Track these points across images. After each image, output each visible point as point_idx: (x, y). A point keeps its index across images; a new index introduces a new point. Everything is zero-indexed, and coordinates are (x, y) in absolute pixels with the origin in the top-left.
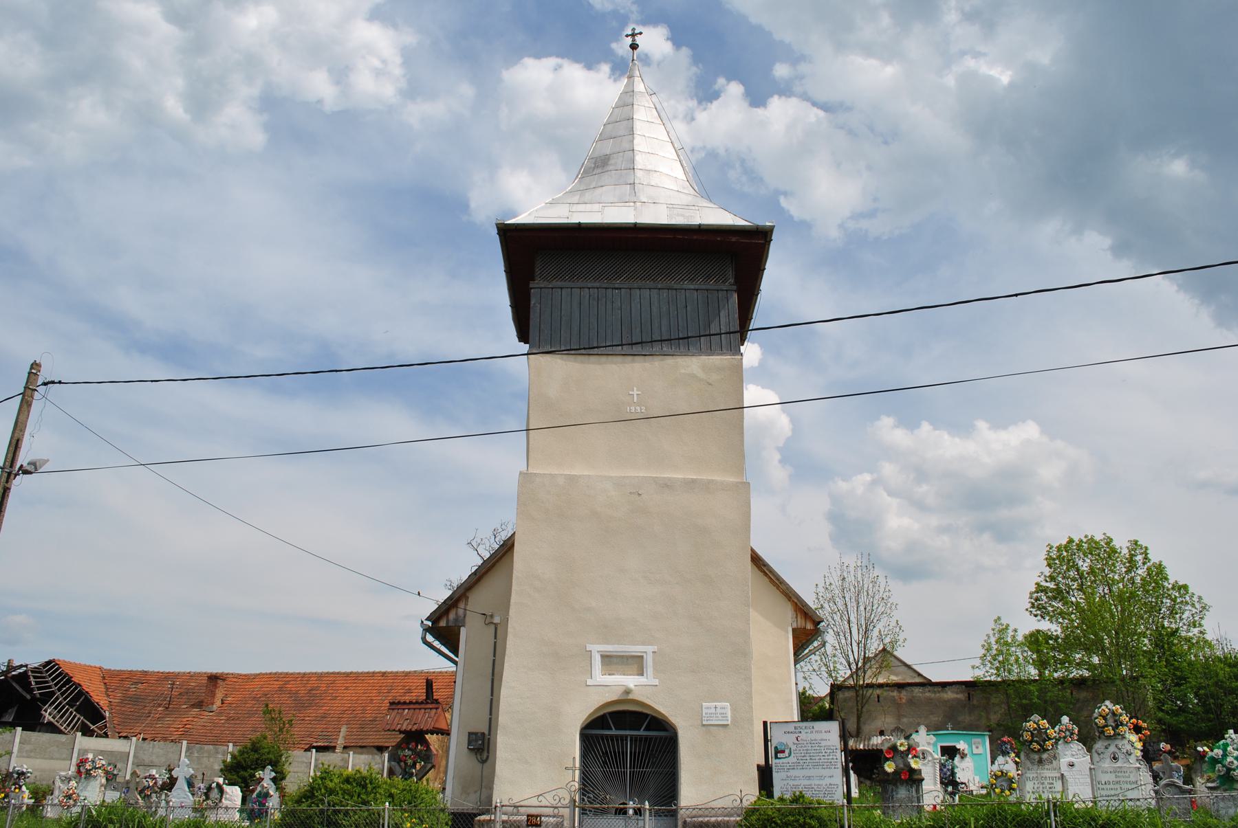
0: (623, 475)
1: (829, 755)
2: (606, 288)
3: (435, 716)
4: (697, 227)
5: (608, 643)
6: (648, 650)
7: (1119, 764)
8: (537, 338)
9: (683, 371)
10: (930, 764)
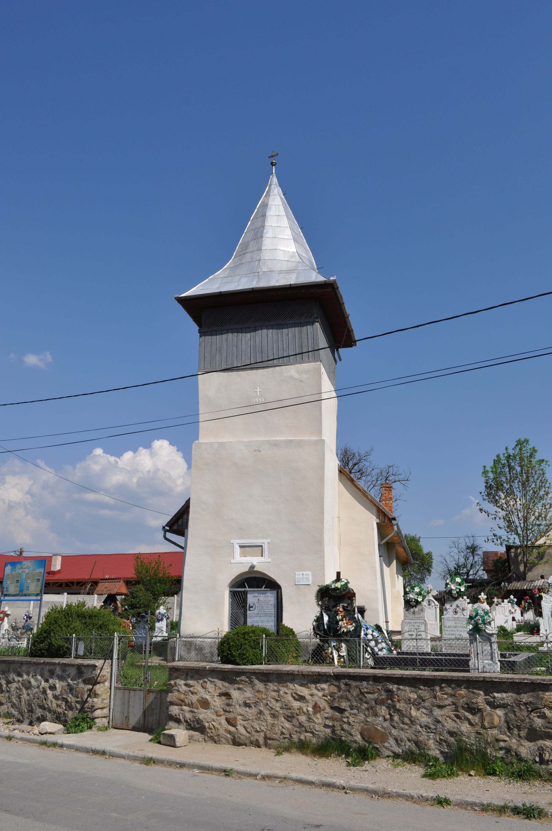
2: (242, 328)
5: (242, 539)
6: (265, 542)
7: (457, 616)
8: (203, 362)
9: (286, 375)
10: (434, 607)
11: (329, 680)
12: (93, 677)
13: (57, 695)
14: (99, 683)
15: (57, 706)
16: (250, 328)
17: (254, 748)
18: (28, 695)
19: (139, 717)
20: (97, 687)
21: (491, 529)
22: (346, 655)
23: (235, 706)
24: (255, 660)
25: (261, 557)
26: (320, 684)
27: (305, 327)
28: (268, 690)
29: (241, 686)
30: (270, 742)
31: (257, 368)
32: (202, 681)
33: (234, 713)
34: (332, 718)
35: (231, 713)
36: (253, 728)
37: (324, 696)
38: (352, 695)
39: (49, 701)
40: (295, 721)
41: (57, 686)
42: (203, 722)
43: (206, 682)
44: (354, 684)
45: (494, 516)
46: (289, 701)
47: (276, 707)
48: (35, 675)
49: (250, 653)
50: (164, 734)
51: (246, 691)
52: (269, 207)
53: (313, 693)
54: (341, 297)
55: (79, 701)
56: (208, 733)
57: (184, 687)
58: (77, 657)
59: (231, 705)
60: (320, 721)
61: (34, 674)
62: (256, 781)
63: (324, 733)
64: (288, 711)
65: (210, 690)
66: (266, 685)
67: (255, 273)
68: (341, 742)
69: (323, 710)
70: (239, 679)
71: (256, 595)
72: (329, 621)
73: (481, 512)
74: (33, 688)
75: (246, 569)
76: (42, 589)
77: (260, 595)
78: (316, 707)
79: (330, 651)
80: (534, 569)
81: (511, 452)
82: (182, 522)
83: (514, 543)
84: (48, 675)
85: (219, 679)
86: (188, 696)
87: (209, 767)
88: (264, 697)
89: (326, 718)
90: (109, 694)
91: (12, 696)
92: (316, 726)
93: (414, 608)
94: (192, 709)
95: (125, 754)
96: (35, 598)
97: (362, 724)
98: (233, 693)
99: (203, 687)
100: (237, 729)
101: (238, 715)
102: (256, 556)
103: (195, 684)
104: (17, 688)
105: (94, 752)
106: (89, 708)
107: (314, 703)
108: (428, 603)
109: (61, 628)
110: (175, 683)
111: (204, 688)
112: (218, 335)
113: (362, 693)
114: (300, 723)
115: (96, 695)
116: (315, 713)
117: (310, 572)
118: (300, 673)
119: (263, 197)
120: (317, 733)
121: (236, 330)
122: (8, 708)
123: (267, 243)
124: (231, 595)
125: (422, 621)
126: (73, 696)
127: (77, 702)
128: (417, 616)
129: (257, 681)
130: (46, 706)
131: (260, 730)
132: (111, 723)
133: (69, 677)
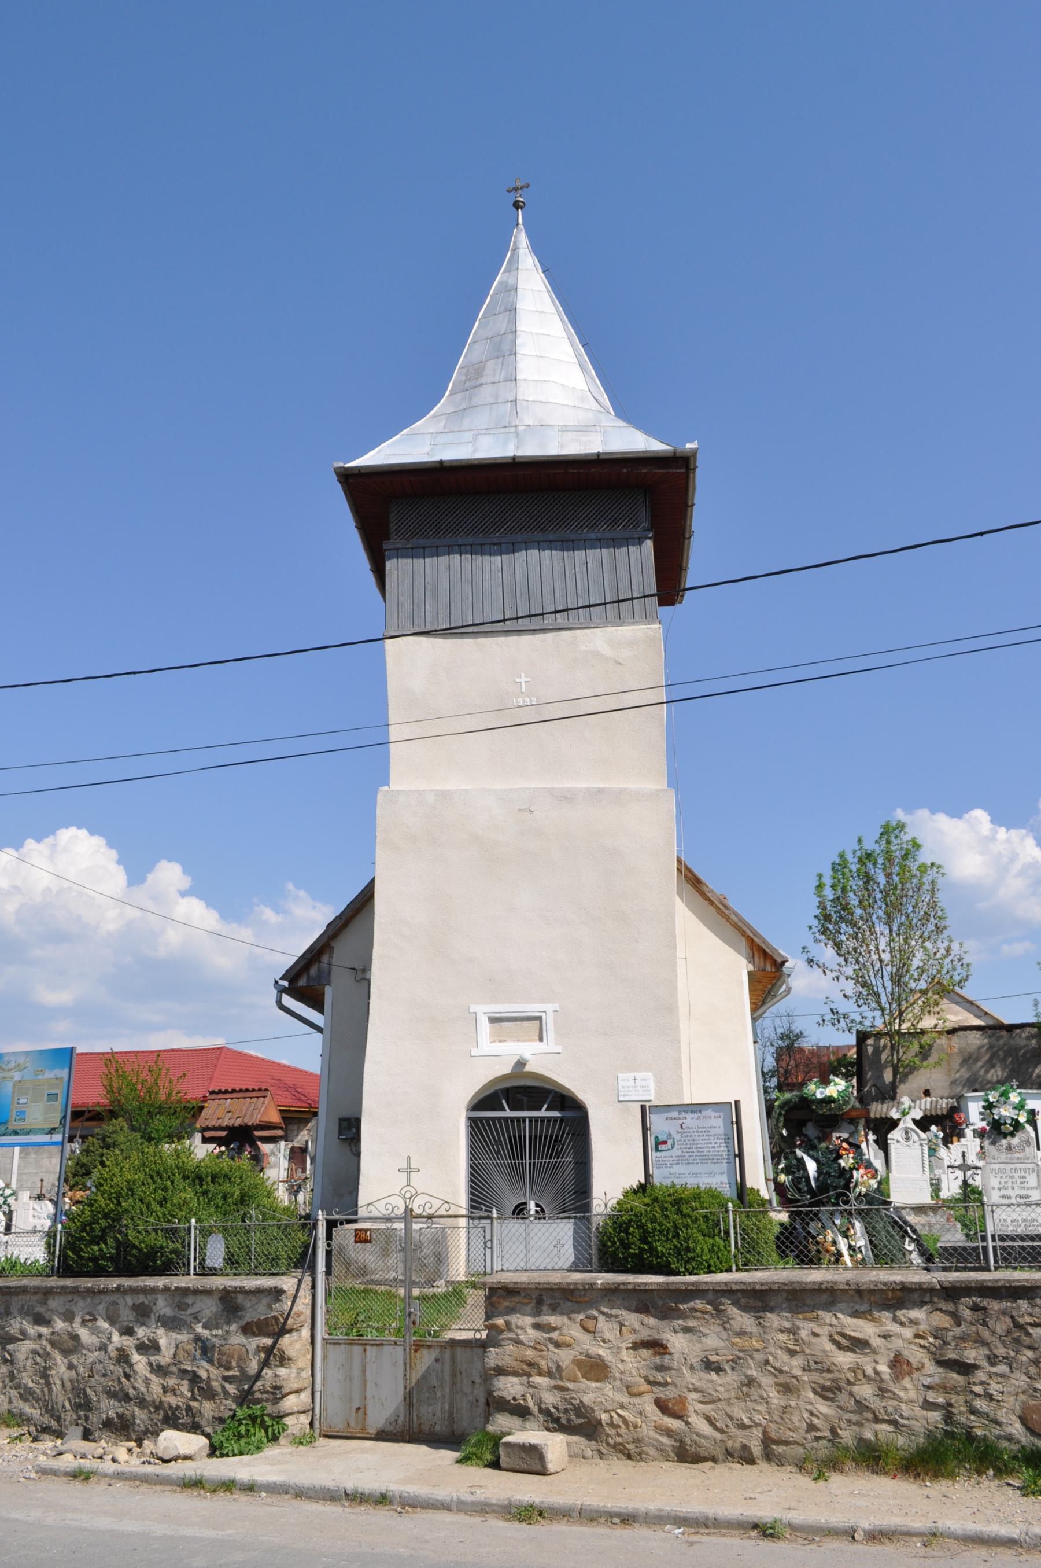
0: (511, 787)
1: (720, 1147)
2: (482, 545)
3: (262, 1107)
4: (595, 457)
6: (547, 1010)
9: (583, 648)
10: (917, 1145)
11: (927, 1299)
12: (275, 1318)
13: (162, 1364)
14: (290, 1331)
15: (165, 1392)
16: (500, 544)
17: (739, 1465)
18: (71, 1367)
19: (393, 1408)
20: (286, 1341)
21: (826, 1000)
22: (865, 1246)
23: (679, 1370)
24: (715, 1263)
25: (538, 1043)
26: (904, 1311)
27: (624, 550)
28: (767, 1330)
29: (691, 1323)
30: (780, 1449)
31: (520, 632)
32: (582, 1316)
33: (676, 1386)
34: (944, 1388)
35: (669, 1387)
36: (731, 1418)
37: (917, 1336)
38: (994, 1332)
39: (140, 1381)
40: (843, 1398)
41: (163, 1342)
42: (594, 1411)
43: (596, 1318)
44: (995, 1306)
45: (835, 974)
46: (824, 1351)
47: (792, 1368)
48: (90, 1320)
49: (702, 1245)
50: (508, 1445)
51: (705, 1335)
52: (519, 291)
53: (887, 1331)
54: (694, 489)
55: (233, 1377)
56: (608, 1435)
57: (530, 1331)
58: (205, 1271)
59: (669, 1369)
60: (912, 1394)
61: (88, 1317)
62: (855, 1546)
63: (925, 1422)
64: (825, 1375)
65: (608, 1335)
66: (758, 1318)
67: (507, 428)
68: (970, 1437)
69: (918, 1369)
70: (685, 1306)
71: (675, 1114)
72: (819, 1171)
73: (811, 966)
74: (84, 1352)
75: (507, 1069)
76: (64, 1117)
77: (684, 1115)
78: (898, 1362)
79: (830, 1238)
80: (910, 1077)
81: (869, 845)
82: (319, 969)
83: (873, 1026)
84: (131, 1318)
85: (630, 1310)
86: (545, 1353)
87: (707, 1518)
88: (757, 1345)
89: (929, 1387)
90: (309, 1357)
91: (19, 1372)
92: (903, 1406)
93: (1009, 1138)
94: (560, 1383)
95: (448, 1498)
96: (46, 1138)
97: (1022, 1397)
98: (672, 1339)
99: (586, 1329)
100: (687, 1423)
101: (690, 1391)
102: (527, 1041)
103: (564, 1325)
104: (35, 1353)
105: (353, 1500)
106: (267, 1392)
107: (892, 1355)
108: (904, 1136)
109: (148, 1206)
110: (508, 1324)
111: (589, 1332)
112: (429, 557)
113: (1017, 1326)
114: (857, 1402)
115: (284, 1360)
116: (897, 1377)
117: (650, 1074)
118: (853, 1287)
119: (501, 271)
120: (905, 1422)
121: (469, 548)
122: (10, 1402)
123: (526, 368)
124: (471, 1126)
125: (1031, 1166)
126: (212, 1364)
127: (226, 1379)
128: (1017, 1155)
129: (735, 1309)
130: (132, 1392)
131: (750, 1423)
132: (317, 1424)
133: (197, 1319)
